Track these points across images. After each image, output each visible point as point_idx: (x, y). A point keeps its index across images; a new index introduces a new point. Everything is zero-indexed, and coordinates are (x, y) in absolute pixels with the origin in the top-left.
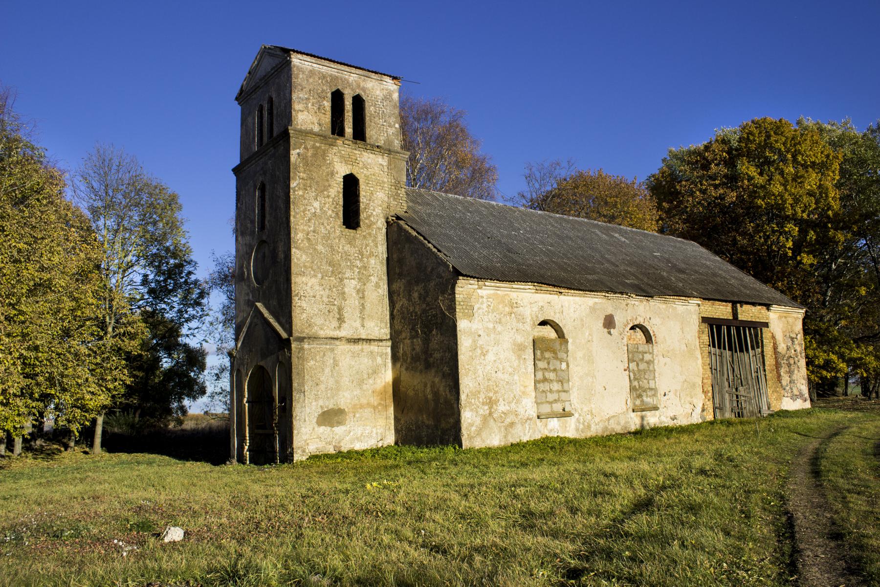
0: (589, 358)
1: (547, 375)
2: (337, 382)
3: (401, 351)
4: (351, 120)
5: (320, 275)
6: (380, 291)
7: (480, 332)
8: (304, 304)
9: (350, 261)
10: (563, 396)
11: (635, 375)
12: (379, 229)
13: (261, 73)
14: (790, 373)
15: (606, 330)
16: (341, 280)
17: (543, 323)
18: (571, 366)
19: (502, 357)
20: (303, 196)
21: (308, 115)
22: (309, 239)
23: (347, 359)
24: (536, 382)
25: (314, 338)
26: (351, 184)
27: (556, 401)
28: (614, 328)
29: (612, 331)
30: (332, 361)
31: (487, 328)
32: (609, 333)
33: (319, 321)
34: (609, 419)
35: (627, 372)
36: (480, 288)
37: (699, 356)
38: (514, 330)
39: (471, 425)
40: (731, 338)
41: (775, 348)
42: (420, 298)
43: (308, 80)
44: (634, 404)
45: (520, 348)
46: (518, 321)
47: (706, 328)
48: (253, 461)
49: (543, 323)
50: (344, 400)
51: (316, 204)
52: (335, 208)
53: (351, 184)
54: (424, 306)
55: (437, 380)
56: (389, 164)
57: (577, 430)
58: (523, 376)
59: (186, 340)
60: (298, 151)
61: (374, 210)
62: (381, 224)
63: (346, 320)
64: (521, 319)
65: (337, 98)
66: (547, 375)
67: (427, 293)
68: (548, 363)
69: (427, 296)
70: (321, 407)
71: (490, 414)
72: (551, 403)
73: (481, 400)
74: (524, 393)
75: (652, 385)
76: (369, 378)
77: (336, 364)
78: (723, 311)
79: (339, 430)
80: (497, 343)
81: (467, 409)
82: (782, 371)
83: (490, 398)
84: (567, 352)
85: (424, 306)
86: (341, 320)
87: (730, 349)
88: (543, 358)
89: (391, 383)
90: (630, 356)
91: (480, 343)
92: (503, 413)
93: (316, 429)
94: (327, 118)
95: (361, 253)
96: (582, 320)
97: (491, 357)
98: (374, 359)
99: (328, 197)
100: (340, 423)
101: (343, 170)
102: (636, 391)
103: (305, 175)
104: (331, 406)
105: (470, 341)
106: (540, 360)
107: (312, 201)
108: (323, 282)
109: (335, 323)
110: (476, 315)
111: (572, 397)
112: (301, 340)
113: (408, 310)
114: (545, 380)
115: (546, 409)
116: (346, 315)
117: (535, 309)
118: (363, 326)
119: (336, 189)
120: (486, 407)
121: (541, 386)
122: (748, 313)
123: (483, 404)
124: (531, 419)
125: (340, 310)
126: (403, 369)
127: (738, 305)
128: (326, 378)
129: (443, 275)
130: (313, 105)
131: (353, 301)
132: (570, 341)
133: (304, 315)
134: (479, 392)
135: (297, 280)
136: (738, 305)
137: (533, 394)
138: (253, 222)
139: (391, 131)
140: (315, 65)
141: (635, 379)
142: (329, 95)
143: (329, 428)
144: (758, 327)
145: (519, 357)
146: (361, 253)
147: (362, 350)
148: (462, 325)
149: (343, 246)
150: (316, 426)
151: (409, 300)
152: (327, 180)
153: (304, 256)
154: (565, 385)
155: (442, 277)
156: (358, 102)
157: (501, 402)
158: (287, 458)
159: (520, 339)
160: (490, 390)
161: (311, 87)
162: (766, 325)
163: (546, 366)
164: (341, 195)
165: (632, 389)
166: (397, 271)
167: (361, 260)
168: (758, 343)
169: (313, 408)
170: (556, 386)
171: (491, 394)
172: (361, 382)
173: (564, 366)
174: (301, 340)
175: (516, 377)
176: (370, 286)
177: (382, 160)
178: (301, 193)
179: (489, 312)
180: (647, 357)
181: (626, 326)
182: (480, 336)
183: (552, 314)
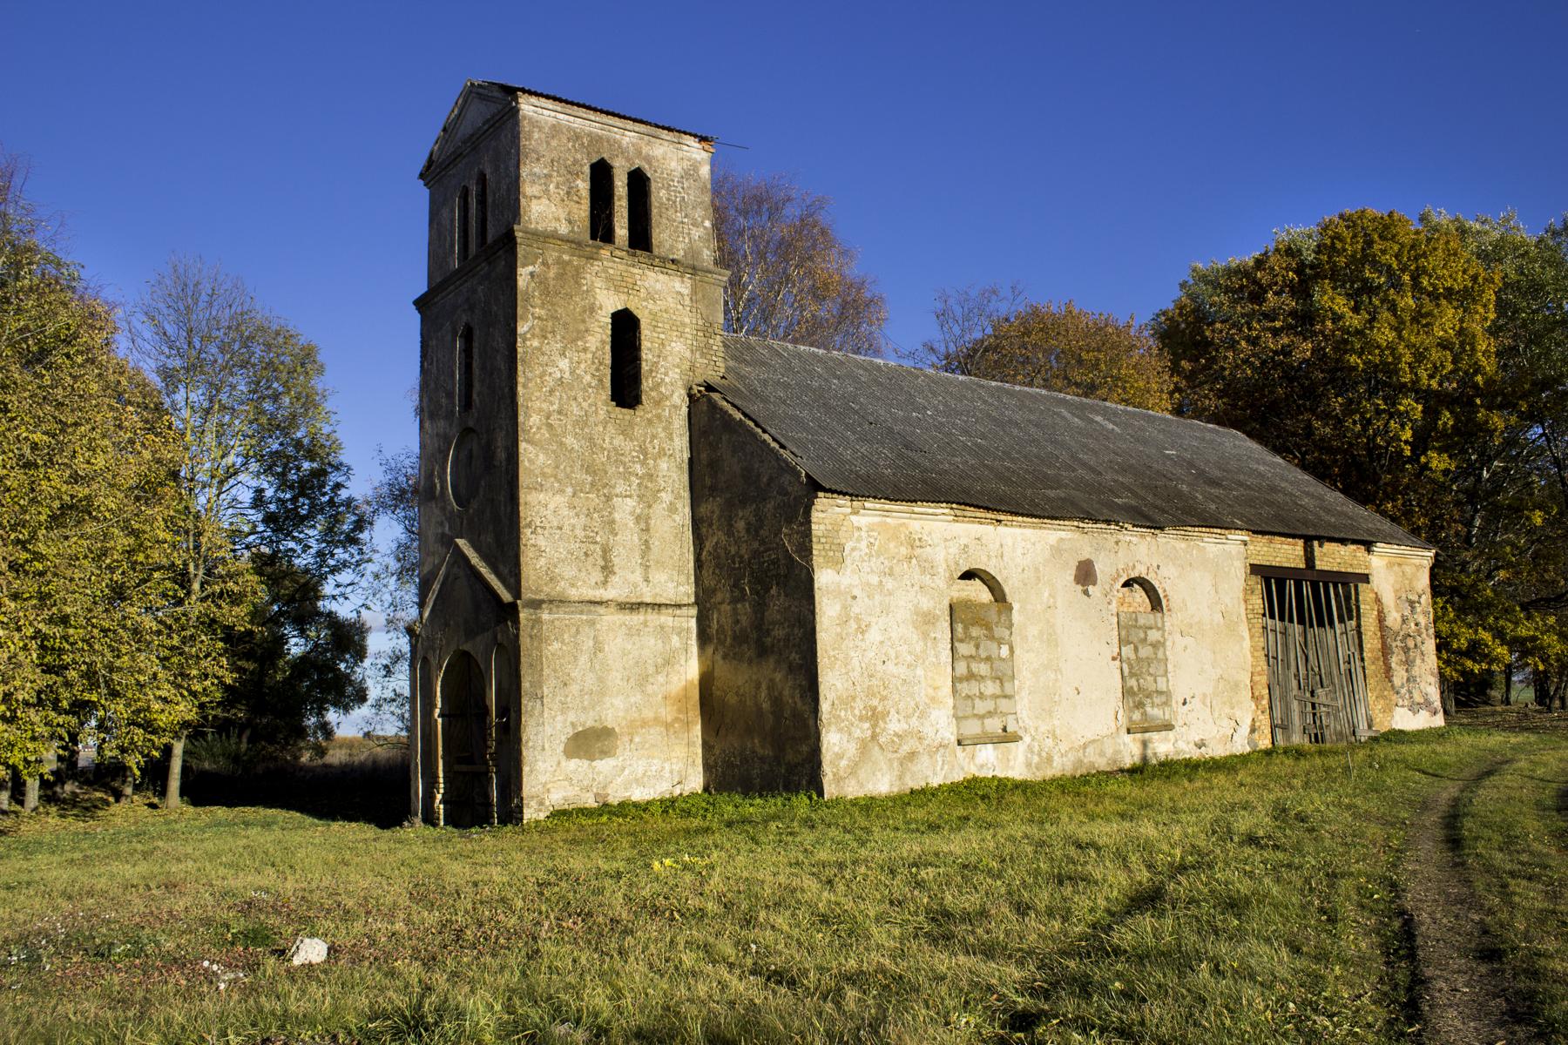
0: (1050, 639)
1: (975, 667)
2: (600, 680)
3: (715, 626)
5: (569, 490)
7: (856, 592)
8: (542, 542)
9: (624, 464)
10: (1004, 704)
11: (1131, 667)
12: (675, 407)
13: (465, 129)
14: (1408, 663)
15: (1080, 588)
16: (608, 498)
17: (968, 575)
18: (1017, 651)
19: (894, 635)
20: (539, 349)
21: (549, 205)
22: (550, 426)
23: (619, 640)
24: (955, 680)
25: (560, 602)
26: (625, 327)
27: (990, 714)
28: (1094, 584)
30: (591, 643)
31: (868, 584)
32: (1086, 593)
33: (568, 571)
34: (1085, 746)
35: (1117, 663)
36: (855, 512)
37: (1246, 635)
38: (917, 588)
39: (840, 756)
40: (1303, 602)
41: (1381, 619)
42: (748, 531)
43: (548, 143)
44: (1130, 719)
45: (927, 619)
47: (1257, 584)
49: (968, 575)
50: (613, 712)
51: (564, 364)
52: (597, 370)
53: (625, 327)
54: (756, 545)
56: (694, 292)
58: (932, 669)
60: (531, 268)
61: (666, 374)
63: (616, 569)
64: (928, 568)
65: (601, 174)
67: (760, 520)
68: (977, 647)
69: (761, 527)
70: (573, 724)
71: (874, 737)
72: (982, 717)
73: (857, 712)
74: (933, 699)
75: (1162, 686)
76: (657, 672)
77: (598, 648)
78: (1288, 553)
79: (604, 765)
80: (885, 610)
81: (833, 728)
82: (1394, 661)
83: (874, 709)
86: (608, 569)
87: (1301, 621)
88: (967, 638)
89: (696, 682)
90: (1123, 633)
91: (856, 610)
92: (896, 734)
93: (563, 763)
94: (583, 211)
96: (1037, 569)
97: (874, 635)
98: (666, 639)
99: (585, 350)
100: (605, 753)
101: (610, 303)
102: (1134, 696)
103: (543, 312)
104: (590, 723)
105: (838, 607)
106: (961, 641)
107: (556, 357)
108: (576, 501)
109: (597, 576)
110: (848, 561)
111: (1019, 707)
112: (536, 605)
113: (727, 553)
114: (971, 676)
115: (972, 728)
116: (616, 561)
117: (953, 550)
118: (647, 580)
119: (599, 337)
121: (964, 688)
122: (1332, 557)
123: (861, 719)
124: (945, 747)
125: (606, 551)
126: (718, 657)
127: (1316, 543)
128: (581, 672)
129: (790, 489)
131: (627, 538)
132: (1016, 606)
133: (542, 561)
134: (854, 699)
135: (529, 498)
137: (951, 702)
138: (450, 395)
139: (696, 233)
140: (561, 116)
141: (1132, 675)
142: (587, 169)
143: (586, 763)
144: (1350, 582)
145: (925, 635)
146: (644, 451)
147: (645, 624)
148: (824, 578)
149: (611, 438)
151: (730, 534)
152: (584, 321)
153: (541, 456)
154: (1007, 685)
156: (639, 181)
157: (893, 715)
158: (512, 815)
159: (926, 603)
160: (874, 695)
161: (554, 155)
162: (1365, 578)
163: (974, 653)
164: (608, 348)
165: (1127, 692)
166: (708, 482)
167: (643, 463)
168: (1350, 610)
169: (559, 726)
170: (990, 688)
171: (875, 702)
172: (643, 681)
173: (1005, 651)
174: (536, 605)
175: (920, 672)
176: (659, 510)
177: (680, 286)
178: (536, 343)
180: (1154, 635)
182: (854, 598)
183: (984, 558)
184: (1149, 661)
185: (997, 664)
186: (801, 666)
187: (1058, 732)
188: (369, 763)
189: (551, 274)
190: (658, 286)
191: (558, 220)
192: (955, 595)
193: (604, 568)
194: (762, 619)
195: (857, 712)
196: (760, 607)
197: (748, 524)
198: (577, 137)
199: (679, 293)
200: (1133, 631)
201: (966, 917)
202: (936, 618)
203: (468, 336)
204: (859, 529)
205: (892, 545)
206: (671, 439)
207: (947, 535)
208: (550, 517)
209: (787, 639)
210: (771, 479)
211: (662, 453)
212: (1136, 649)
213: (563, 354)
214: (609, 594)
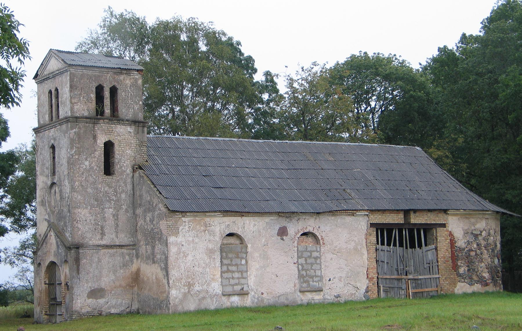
0: (265, 257)
2: (100, 272)
4: (109, 100)
5: (89, 207)
6: (128, 215)
8: (80, 226)
9: (109, 197)
10: (243, 281)
11: (303, 266)
12: (128, 174)
15: (279, 237)
16: (103, 209)
18: (249, 262)
19: (198, 257)
20: (78, 159)
22: (82, 186)
23: (107, 258)
24: (222, 272)
26: (109, 147)
27: (236, 284)
28: (287, 235)
29: (284, 238)
30: (97, 260)
32: (282, 239)
33: (89, 235)
34: (279, 297)
35: (296, 265)
36: (184, 217)
37: (365, 252)
38: (207, 241)
41: (452, 242)
42: (150, 221)
43: (80, 82)
46: (210, 235)
49: (231, 235)
51: (87, 163)
53: (109, 147)
57: (253, 303)
59: (32, 280)
60: (74, 130)
61: (124, 163)
62: (129, 171)
63: (106, 234)
65: (99, 90)
68: (231, 261)
71: (189, 292)
72: (233, 285)
73: (183, 283)
74: (213, 279)
75: (318, 273)
77: (99, 261)
79: (101, 301)
84: (247, 253)
85: (152, 226)
86: (103, 234)
87: (401, 245)
88: (227, 258)
90: (300, 254)
92: (197, 291)
93: (87, 300)
94: (93, 105)
95: (115, 191)
96: (259, 231)
97: (190, 258)
98: (124, 257)
99: (95, 157)
100: (102, 297)
101: (101, 140)
104: (96, 287)
105: (176, 249)
106: (225, 259)
108: (92, 211)
109: (99, 236)
110: (181, 233)
111: (249, 282)
114: (228, 271)
115: (229, 289)
116: (106, 231)
117: (223, 227)
121: (225, 275)
123: (184, 286)
124: (217, 295)
125: (102, 228)
130: (84, 97)
132: (249, 246)
134: (182, 279)
137: (220, 280)
139: (136, 107)
141: (303, 270)
142: (94, 90)
143: (95, 300)
145: (210, 257)
146: (115, 191)
150: (87, 299)
152: (94, 147)
153: (79, 197)
155: (160, 210)
156: (114, 91)
159: (210, 246)
160: (189, 278)
164: (103, 155)
165: (300, 276)
166: (139, 202)
167: (116, 196)
169: (85, 288)
171: (190, 280)
173: (243, 262)
175: (208, 270)
176: (122, 212)
177: (130, 129)
178: (77, 157)
179: (189, 231)
180: (315, 254)
181: (296, 234)
182: (183, 245)
183: (236, 229)
184: (312, 264)
185: (240, 267)
189: (82, 131)
190: (122, 130)
191: (84, 110)
193: (101, 234)
195: (183, 283)
196: (153, 247)
200: (304, 253)
202: (215, 251)
203: (53, 147)
204: (185, 222)
205: (198, 227)
206: (126, 186)
207: (220, 225)
208: (82, 217)
209: (160, 259)
210: (156, 204)
211: (123, 191)
212: (306, 260)
213: (86, 160)
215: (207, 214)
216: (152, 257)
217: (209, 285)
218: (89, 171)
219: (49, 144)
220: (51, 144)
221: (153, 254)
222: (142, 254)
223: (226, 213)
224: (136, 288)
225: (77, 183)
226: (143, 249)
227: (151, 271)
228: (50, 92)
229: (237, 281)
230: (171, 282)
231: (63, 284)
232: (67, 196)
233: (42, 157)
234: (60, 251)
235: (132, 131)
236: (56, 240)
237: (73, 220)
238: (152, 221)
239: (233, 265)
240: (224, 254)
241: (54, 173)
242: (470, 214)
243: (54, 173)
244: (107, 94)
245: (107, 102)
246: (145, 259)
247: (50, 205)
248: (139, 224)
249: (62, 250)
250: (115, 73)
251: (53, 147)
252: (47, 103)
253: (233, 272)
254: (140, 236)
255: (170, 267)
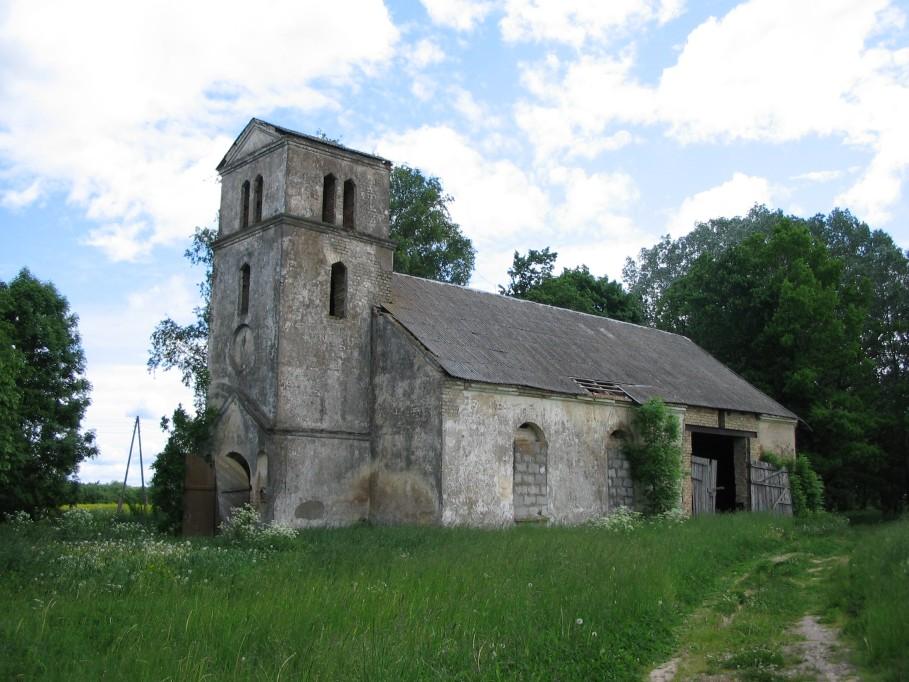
3: (381, 447)
4: (342, 199)
10: (541, 500)
13: (249, 146)
16: (325, 371)
24: (515, 485)
27: (533, 505)
30: (312, 453)
33: (301, 411)
36: (466, 389)
38: (497, 432)
42: (404, 395)
48: (828, 508)
49: (525, 426)
53: (339, 270)
55: (417, 478)
58: (503, 477)
64: (504, 421)
65: (329, 182)
66: (525, 477)
67: (412, 390)
68: (528, 467)
70: (301, 499)
71: (470, 513)
74: (502, 495)
81: (448, 508)
83: (470, 499)
88: (523, 461)
91: (464, 443)
92: (482, 513)
94: (318, 204)
96: (563, 423)
97: (472, 458)
101: (332, 258)
109: (317, 415)
112: (287, 432)
113: (391, 406)
114: (523, 483)
117: (518, 411)
119: (325, 276)
120: (466, 508)
121: (519, 489)
127: (726, 415)
129: (431, 374)
130: (306, 190)
136: (726, 415)
142: (323, 181)
145: (500, 460)
150: (294, 518)
154: (543, 489)
156: (349, 187)
157: (480, 503)
159: (500, 441)
162: (755, 435)
167: (345, 352)
170: (534, 490)
177: (371, 249)
178: (290, 281)
183: (534, 417)
186: (431, 474)
187: (265, 492)
188: (727, 512)
192: (517, 436)
194: (410, 445)
196: (409, 438)
197: (405, 391)
198: (318, 161)
199: (369, 253)
201: (483, 347)
204: (467, 398)
207: (516, 407)
209: (425, 457)
214: (325, 425)
215: (500, 388)
216: (405, 454)
217: (497, 502)
218: (308, 306)
219: (238, 265)
220: (242, 264)
221: (409, 450)
222: (385, 449)
223: (525, 390)
224: (368, 503)
225: (288, 324)
226: (390, 440)
227: (403, 482)
228: (246, 185)
229: (533, 499)
230: (445, 496)
231: (254, 491)
232: (269, 343)
233: (222, 287)
234: (251, 436)
235: (373, 252)
236: (243, 416)
237: (277, 386)
238: (407, 394)
239: (530, 474)
240: (518, 455)
241: (244, 310)
242: (780, 422)
243: (244, 310)
244: (340, 190)
245: (339, 202)
246: (389, 457)
247: (233, 363)
248: (380, 400)
249: (253, 435)
250: (353, 161)
251: (246, 269)
252: (239, 202)
253: (529, 485)
254: (379, 420)
255: (445, 470)
